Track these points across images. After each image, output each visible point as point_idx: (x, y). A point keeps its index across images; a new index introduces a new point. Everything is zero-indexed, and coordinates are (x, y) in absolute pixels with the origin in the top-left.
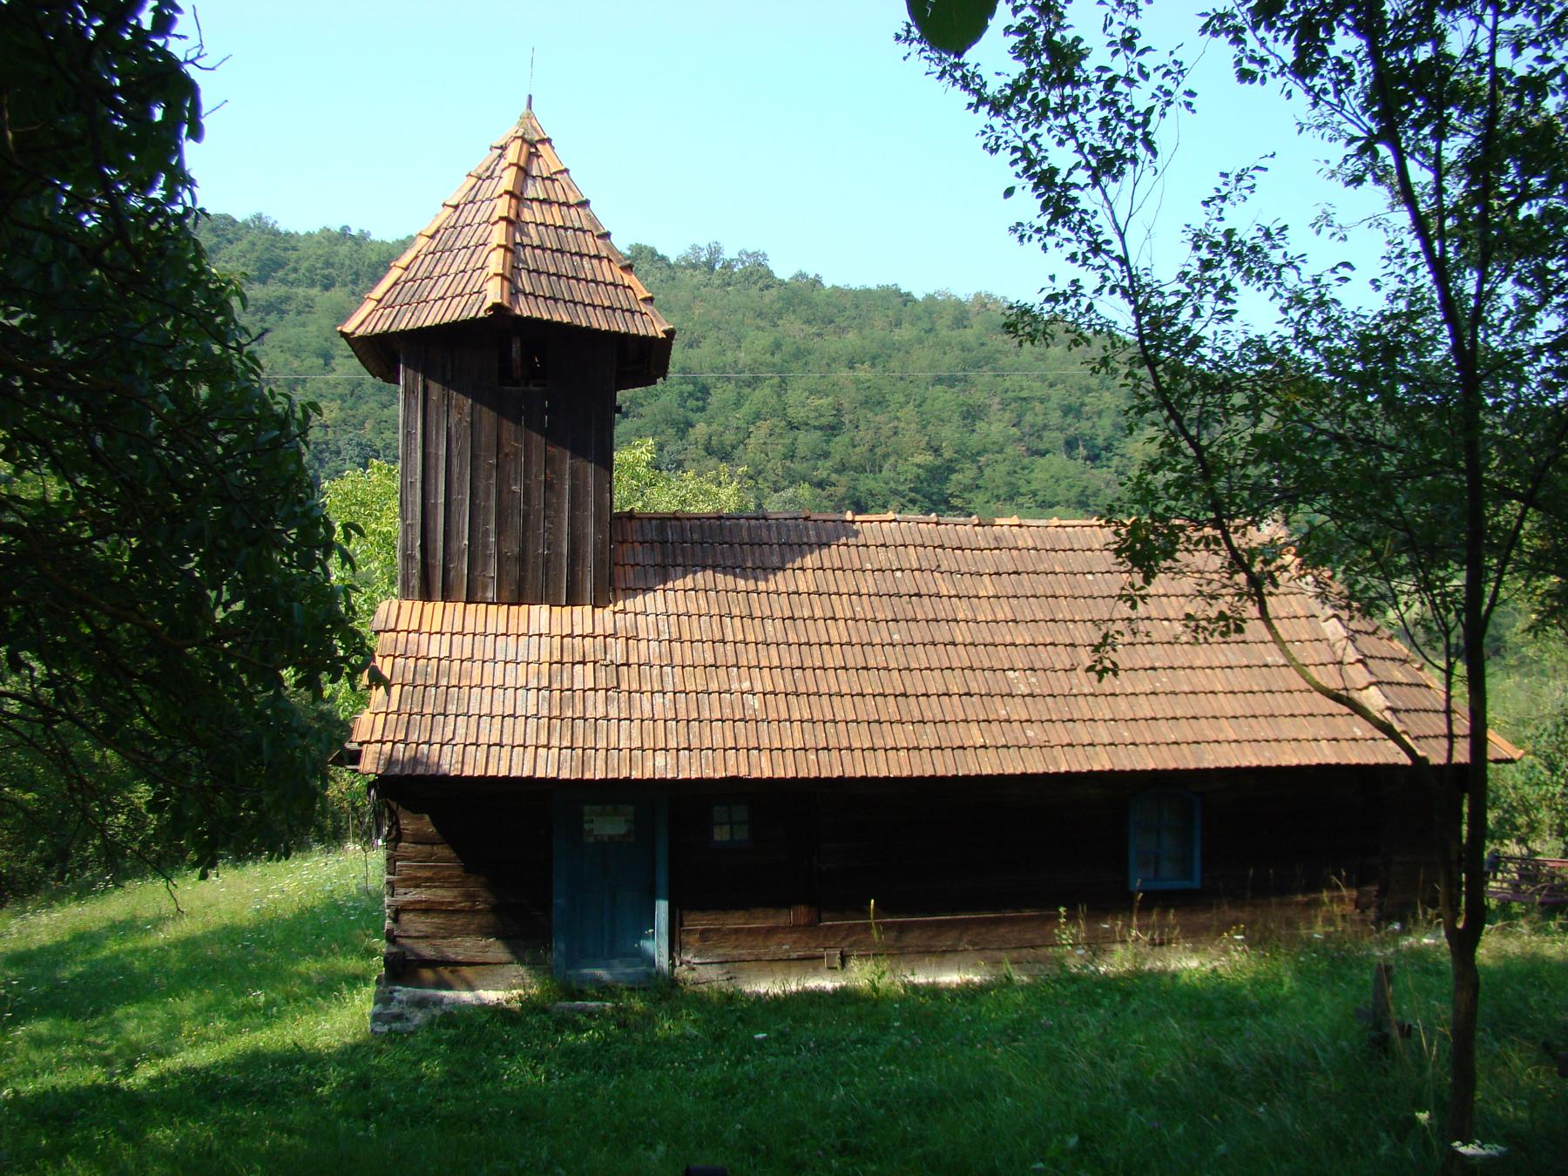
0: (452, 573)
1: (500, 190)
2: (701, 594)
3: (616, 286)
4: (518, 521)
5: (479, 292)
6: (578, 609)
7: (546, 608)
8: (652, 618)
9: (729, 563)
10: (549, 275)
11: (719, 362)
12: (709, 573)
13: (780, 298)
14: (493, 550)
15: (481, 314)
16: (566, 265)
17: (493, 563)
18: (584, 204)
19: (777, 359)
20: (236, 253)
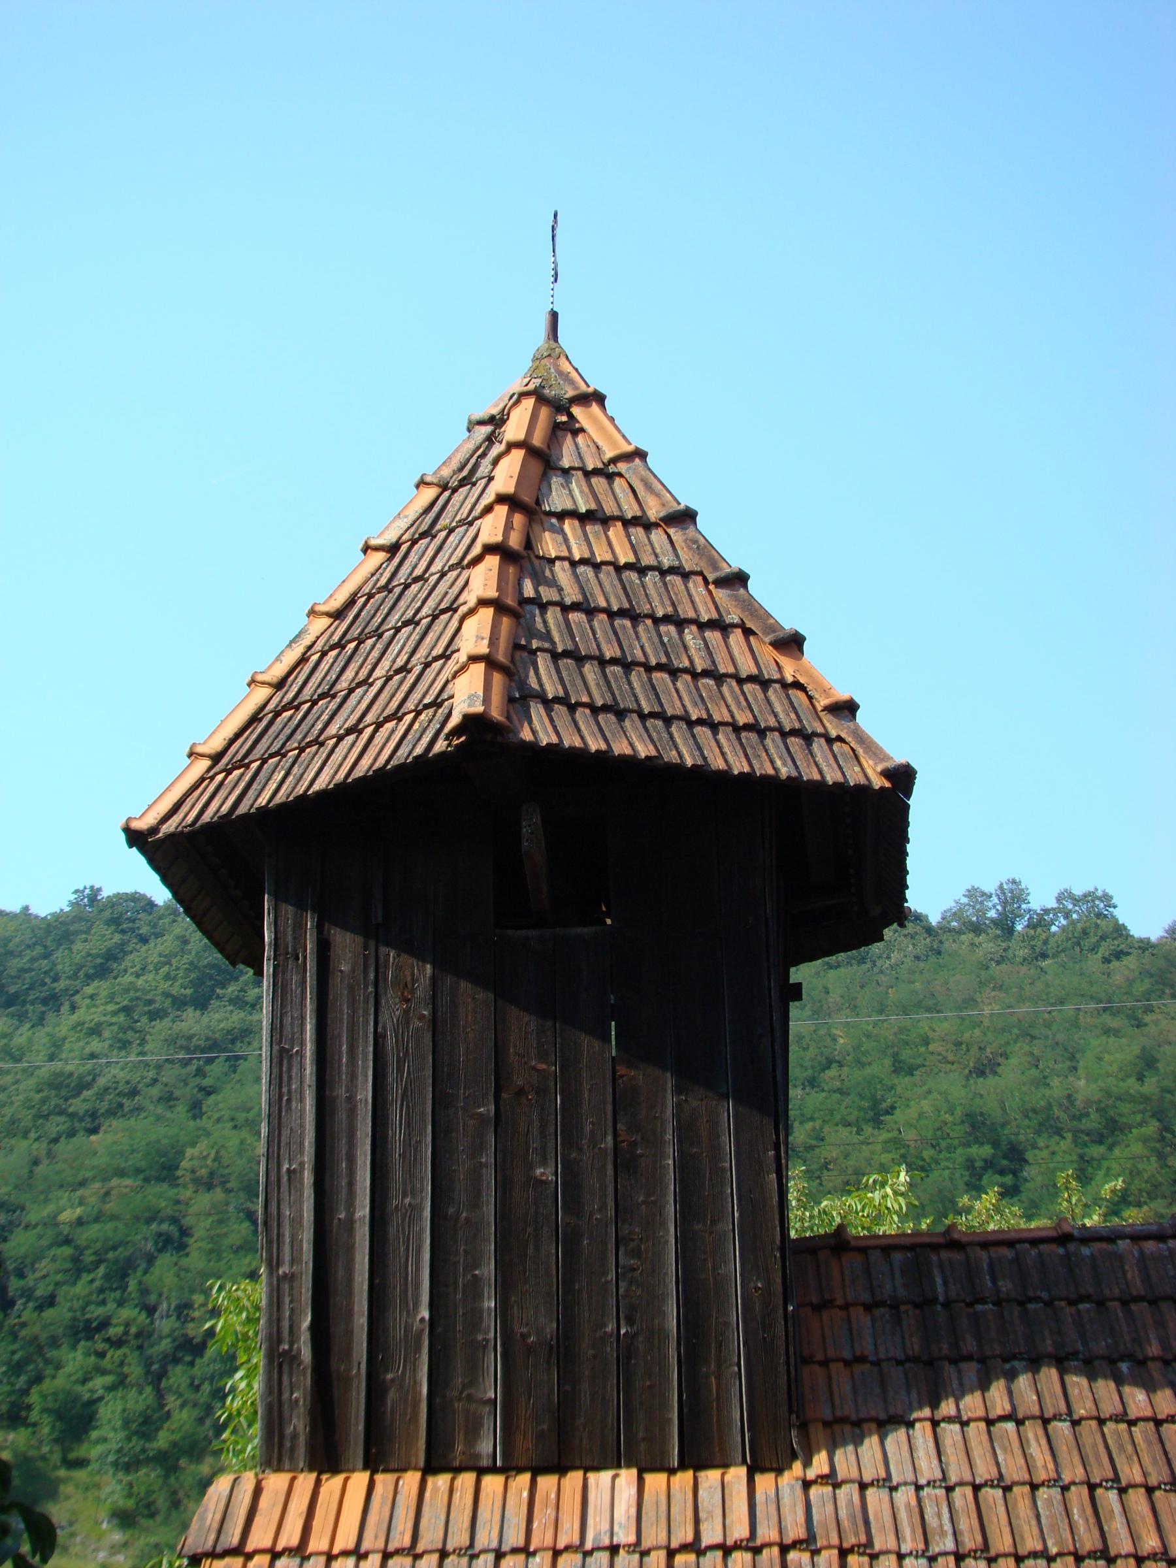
0: (392, 1395)
1: (488, 498)
2: (1032, 1431)
3: (765, 684)
4: (552, 1252)
5: (436, 704)
6: (710, 1477)
7: (627, 1477)
8: (905, 1496)
9: (1100, 1347)
10: (603, 662)
11: (1037, 1099)
12: (1049, 1375)
13: (1145, 973)
14: (491, 1331)
15: (440, 746)
16: (643, 643)
17: (493, 1363)
18: (686, 517)
19: (1150, 1086)
20: (154, 958)
